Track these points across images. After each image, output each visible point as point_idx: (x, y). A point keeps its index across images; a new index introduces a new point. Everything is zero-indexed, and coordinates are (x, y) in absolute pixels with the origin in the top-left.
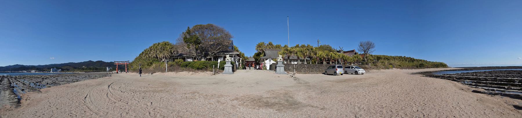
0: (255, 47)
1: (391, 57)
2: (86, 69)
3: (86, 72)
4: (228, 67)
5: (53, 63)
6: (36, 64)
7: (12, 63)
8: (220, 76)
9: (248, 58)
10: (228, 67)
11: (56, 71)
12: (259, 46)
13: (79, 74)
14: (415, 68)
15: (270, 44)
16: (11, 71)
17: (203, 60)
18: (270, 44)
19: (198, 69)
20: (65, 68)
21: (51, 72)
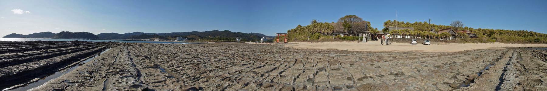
0: (383, 24)
1: (505, 31)
2: (212, 39)
3: (216, 42)
4: (364, 39)
5: (175, 31)
6: (157, 32)
7: (132, 31)
8: (361, 43)
9: (378, 32)
10: (364, 39)
11: (182, 40)
12: (386, 24)
13: (205, 44)
14: (527, 43)
15: (395, 22)
16: (132, 39)
17: (351, 36)
18: (395, 22)
19: (351, 40)
20: (190, 37)
21: (177, 41)
